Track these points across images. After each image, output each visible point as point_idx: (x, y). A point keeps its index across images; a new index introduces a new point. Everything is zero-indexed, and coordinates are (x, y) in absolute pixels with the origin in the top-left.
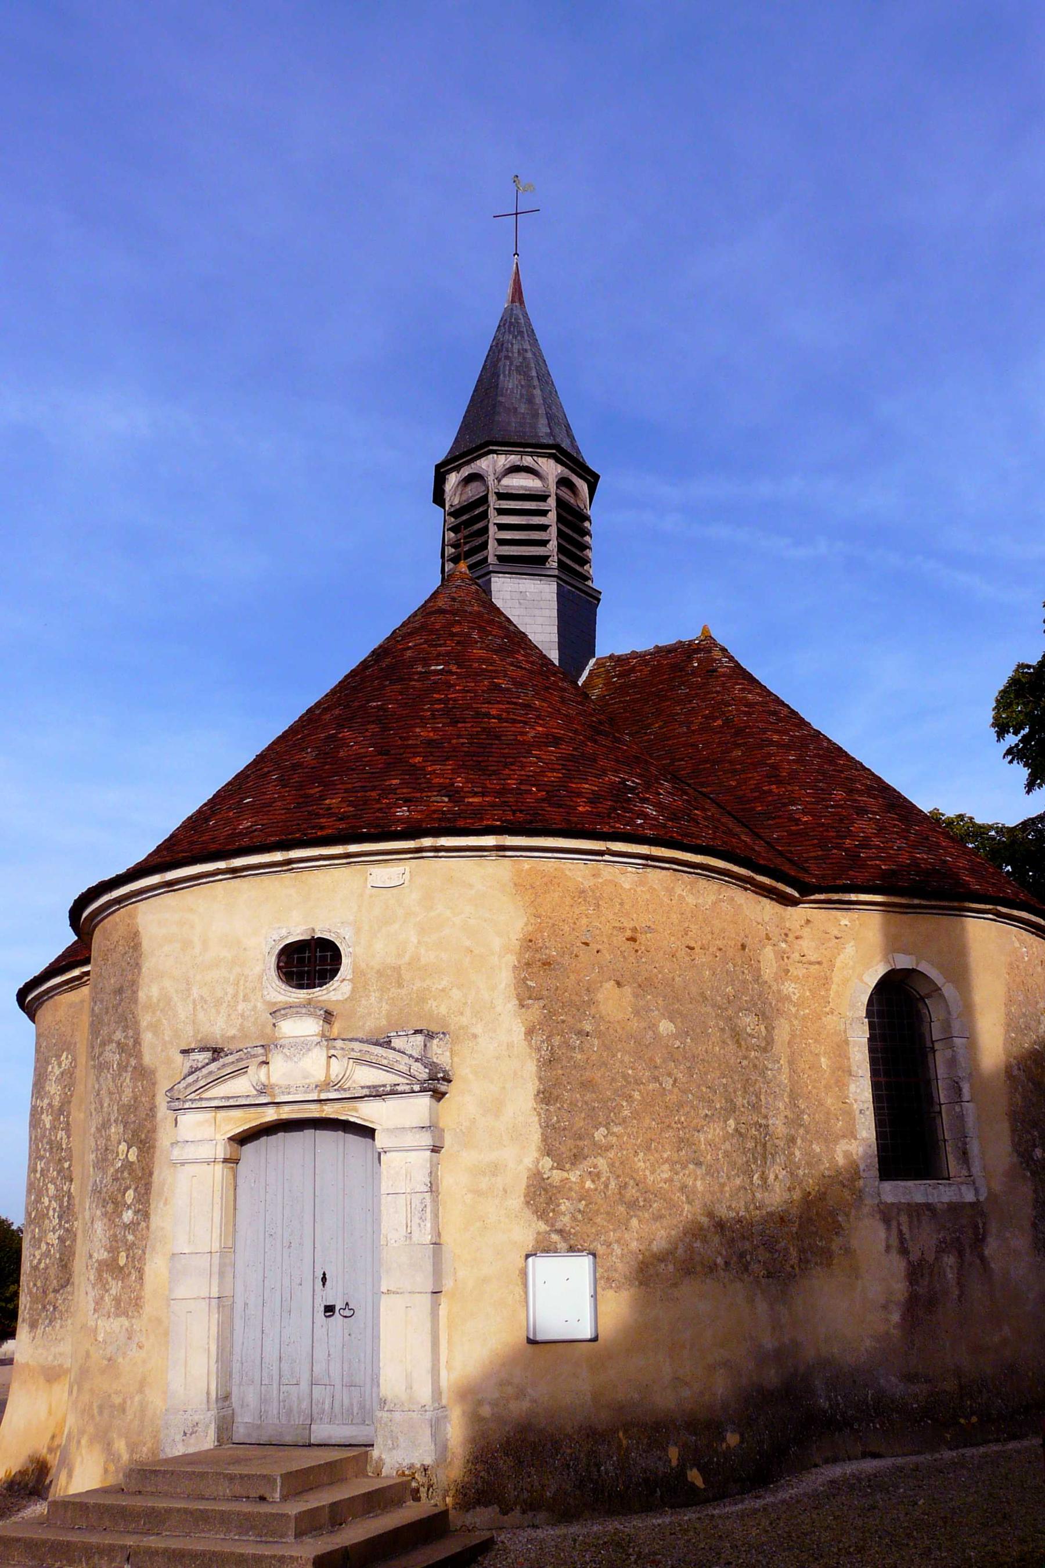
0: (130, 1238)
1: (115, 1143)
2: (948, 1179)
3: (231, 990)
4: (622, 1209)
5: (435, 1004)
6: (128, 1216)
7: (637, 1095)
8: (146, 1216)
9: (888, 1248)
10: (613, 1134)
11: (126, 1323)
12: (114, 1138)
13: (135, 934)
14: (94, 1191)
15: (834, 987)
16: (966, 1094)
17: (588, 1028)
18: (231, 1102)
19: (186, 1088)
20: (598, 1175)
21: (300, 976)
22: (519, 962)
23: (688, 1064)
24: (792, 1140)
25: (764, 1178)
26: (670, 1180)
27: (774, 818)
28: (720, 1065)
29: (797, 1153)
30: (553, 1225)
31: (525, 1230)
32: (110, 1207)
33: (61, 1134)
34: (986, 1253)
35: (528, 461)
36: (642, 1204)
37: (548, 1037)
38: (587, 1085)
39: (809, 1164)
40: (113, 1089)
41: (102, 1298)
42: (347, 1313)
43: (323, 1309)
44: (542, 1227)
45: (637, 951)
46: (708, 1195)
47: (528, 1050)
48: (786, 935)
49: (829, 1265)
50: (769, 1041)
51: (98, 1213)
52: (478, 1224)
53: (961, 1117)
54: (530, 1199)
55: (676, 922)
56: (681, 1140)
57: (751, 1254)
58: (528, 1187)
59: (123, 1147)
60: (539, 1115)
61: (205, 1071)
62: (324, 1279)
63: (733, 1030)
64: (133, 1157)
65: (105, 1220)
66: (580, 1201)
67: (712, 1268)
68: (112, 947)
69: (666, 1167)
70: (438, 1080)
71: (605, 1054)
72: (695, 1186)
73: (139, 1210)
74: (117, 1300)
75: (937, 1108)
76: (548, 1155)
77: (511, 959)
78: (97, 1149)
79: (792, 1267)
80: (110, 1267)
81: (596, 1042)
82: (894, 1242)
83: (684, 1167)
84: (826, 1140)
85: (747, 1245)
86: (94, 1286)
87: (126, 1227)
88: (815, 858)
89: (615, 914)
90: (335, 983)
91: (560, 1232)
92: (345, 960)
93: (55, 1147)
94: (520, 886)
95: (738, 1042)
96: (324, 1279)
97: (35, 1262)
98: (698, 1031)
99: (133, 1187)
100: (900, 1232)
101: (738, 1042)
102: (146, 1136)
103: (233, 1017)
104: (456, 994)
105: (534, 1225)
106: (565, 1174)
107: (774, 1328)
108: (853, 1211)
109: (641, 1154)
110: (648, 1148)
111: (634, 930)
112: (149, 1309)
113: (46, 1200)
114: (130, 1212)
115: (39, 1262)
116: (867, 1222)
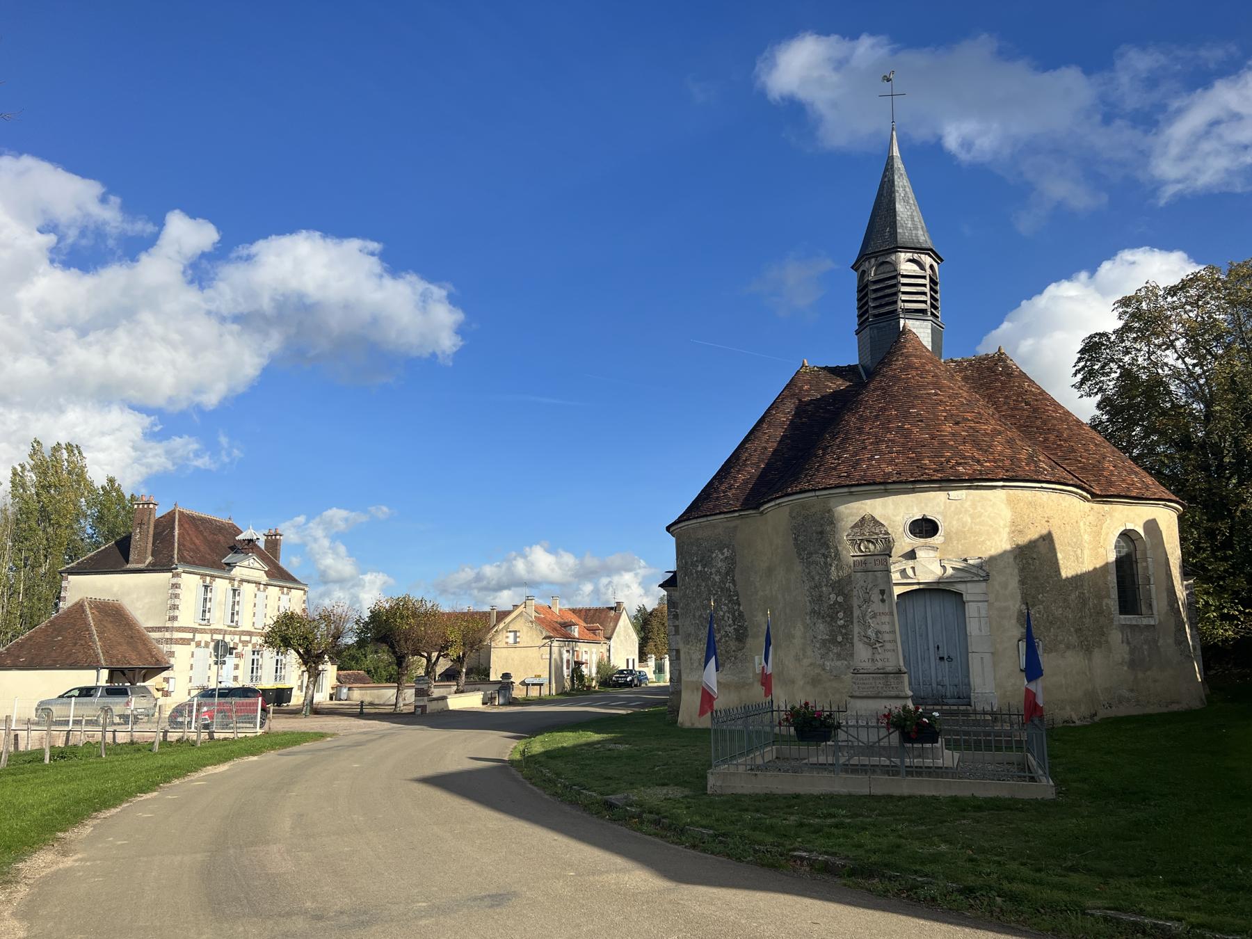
21: (921, 532)
32: (828, 619)
38: (1036, 578)
53: (1149, 590)
77: (1007, 530)
94: (1009, 501)
104: (988, 543)
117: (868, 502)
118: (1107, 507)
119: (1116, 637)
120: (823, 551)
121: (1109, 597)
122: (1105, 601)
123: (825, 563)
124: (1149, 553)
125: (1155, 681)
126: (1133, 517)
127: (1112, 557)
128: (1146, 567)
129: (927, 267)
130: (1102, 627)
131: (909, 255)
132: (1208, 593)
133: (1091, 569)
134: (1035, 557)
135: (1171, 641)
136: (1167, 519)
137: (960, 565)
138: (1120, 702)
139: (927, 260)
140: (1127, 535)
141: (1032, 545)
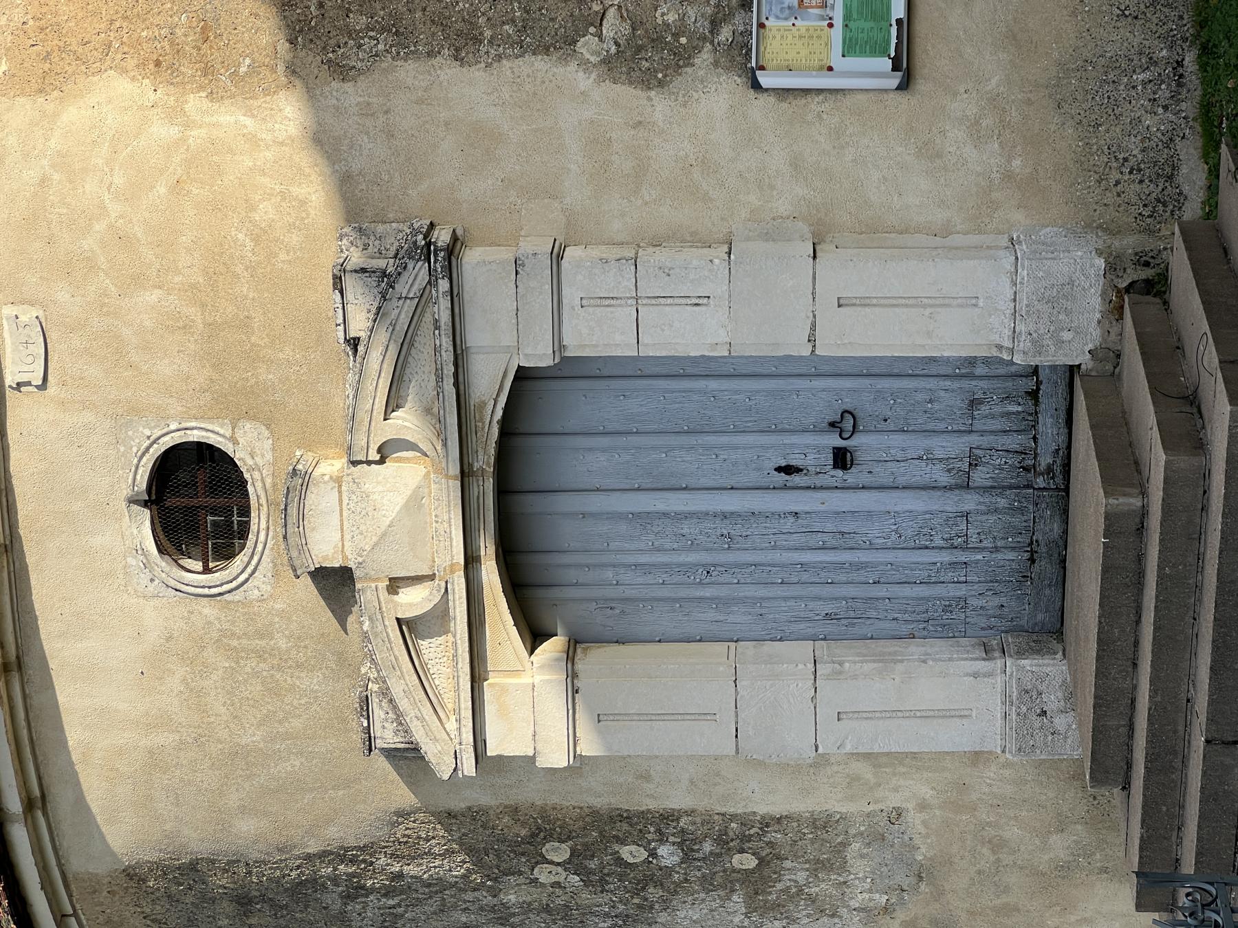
0: (707, 847)
3: (250, 665)
6: (668, 855)
8: (669, 817)
11: (856, 846)
13: (130, 877)
18: (457, 319)
22: (201, 88)
31: (712, 96)
32: (653, 893)
37: (350, 37)
40: (433, 905)
41: (812, 900)
43: (839, 473)
44: (705, 57)
52: (696, 174)
54: (649, 81)
58: (631, 83)
59: (543, 875)
60: (499, 57)
61: (403, 704)
62: (788, 470)
64: (559, 852)
70: (428, 244)
73: (659, 831)
76: (575, 42)
77: (195, 103)
87: (687, 858)
90: (240, 456)
91: (715, 25)
92: (195, 436)
99: (616, 847)
102: (524, 824)
103: (301, 657)
104: (266, 211)
105: (701, 73)
106: (612, 12)
112: (826, 798)
114: (663, 851)
117: (75, 736)
120: (332, 899)
123: (388, 892)
137: (379, 363)
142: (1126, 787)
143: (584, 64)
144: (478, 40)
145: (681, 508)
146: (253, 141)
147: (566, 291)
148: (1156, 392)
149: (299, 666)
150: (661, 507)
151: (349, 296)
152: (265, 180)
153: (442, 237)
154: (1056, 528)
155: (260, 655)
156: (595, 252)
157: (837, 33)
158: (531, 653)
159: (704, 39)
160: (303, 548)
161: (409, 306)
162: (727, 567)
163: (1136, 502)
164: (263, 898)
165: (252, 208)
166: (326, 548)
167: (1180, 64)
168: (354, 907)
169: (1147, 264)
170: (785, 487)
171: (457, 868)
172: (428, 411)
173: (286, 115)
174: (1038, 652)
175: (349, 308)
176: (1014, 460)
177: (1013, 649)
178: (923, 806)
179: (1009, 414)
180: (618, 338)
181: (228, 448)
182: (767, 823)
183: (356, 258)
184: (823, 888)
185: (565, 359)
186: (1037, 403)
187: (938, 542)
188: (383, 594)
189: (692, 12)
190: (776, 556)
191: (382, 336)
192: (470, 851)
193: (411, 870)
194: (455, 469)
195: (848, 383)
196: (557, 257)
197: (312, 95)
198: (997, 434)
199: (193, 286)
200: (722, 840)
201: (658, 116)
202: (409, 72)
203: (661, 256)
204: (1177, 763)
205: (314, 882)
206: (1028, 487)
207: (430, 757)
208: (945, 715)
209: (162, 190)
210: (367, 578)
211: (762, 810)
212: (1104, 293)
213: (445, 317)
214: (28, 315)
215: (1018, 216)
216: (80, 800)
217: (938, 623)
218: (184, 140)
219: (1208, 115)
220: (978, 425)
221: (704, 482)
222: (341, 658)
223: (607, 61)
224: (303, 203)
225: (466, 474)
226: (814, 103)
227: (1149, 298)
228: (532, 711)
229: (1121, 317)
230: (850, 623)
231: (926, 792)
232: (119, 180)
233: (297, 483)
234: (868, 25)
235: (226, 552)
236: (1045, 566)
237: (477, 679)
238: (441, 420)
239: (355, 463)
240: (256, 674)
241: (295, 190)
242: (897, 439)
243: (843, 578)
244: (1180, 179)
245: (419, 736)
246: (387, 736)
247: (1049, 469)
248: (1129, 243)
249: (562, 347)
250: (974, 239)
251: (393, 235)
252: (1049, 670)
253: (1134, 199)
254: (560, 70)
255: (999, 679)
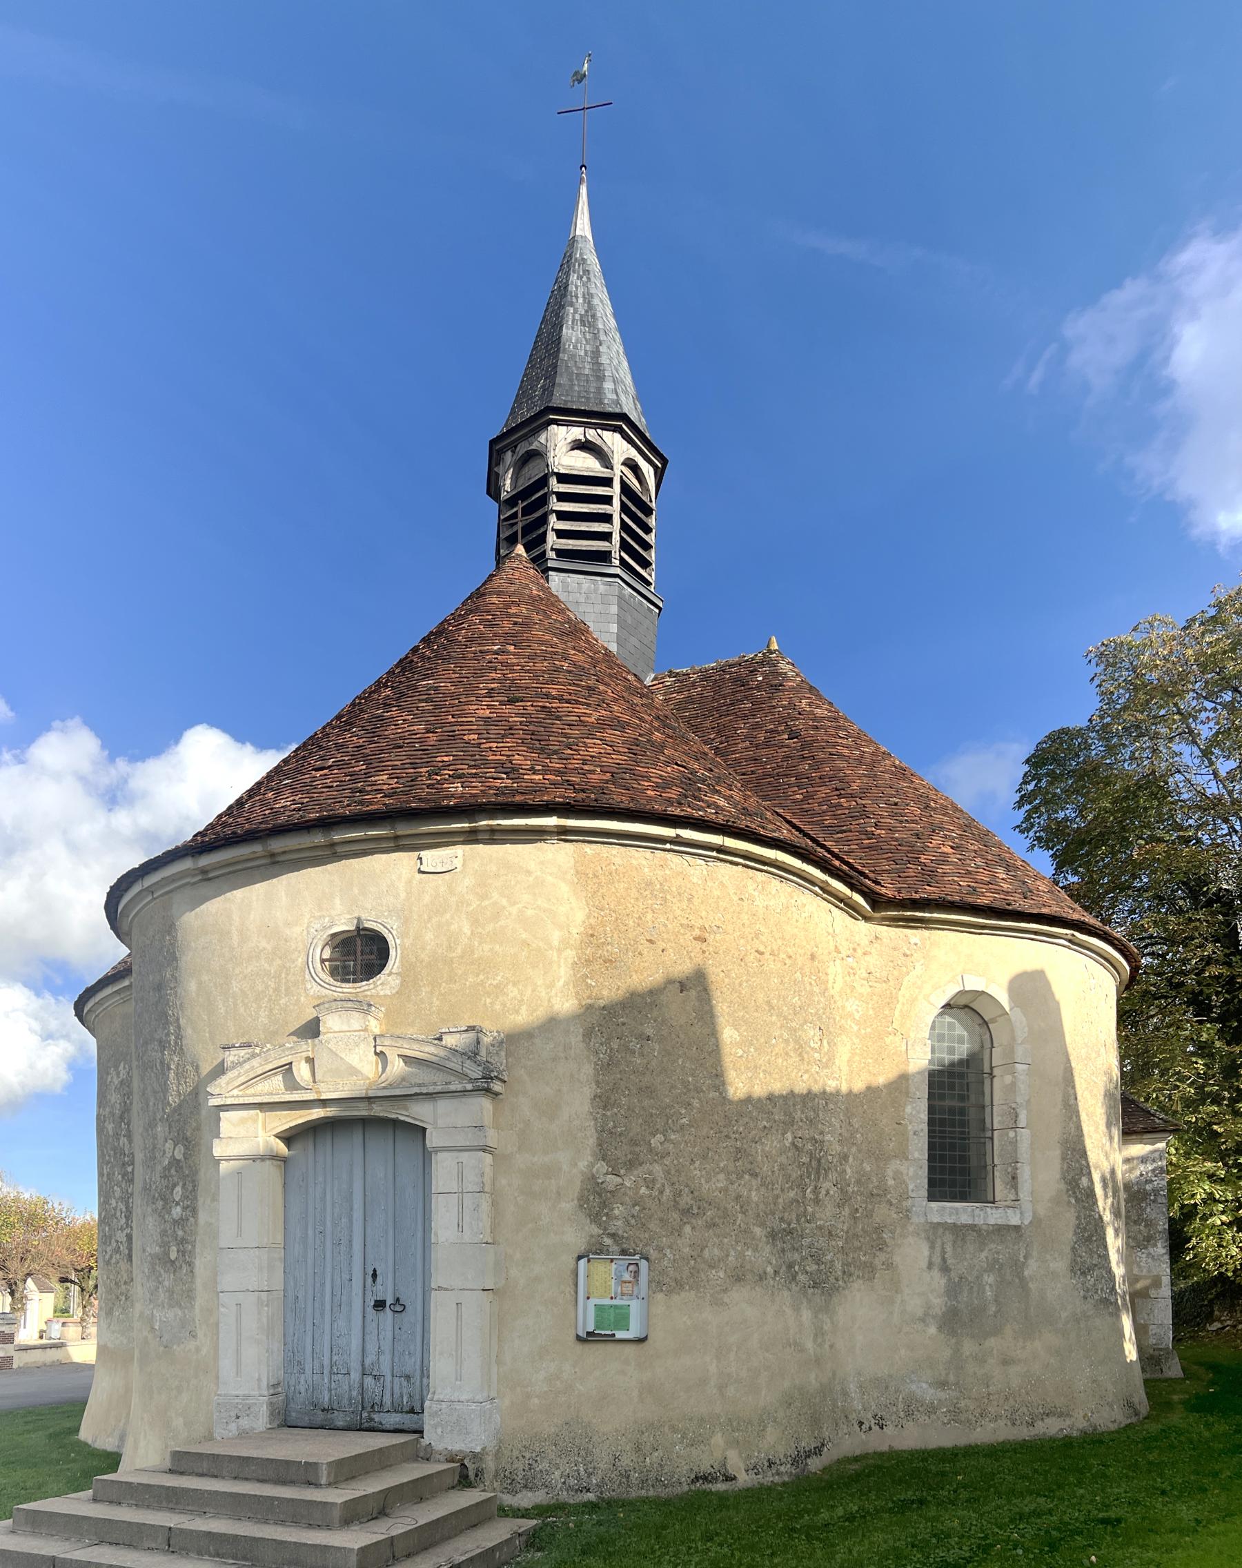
0: (180, 1233)
1: (161, 1141)
2: (993, 1203)
4: (676, 1215)
5: (488, 1001)
6: (177, 1211)
7: (696, 1103)
8: (194, 1212)
9: (930, 1266)
10: (671, 1141)
12: (161, 1136)
14: (145, 1189)
15: (899, 1007)
16: (1022, 1121)
17: (649, 1031)
19: (228, 1083)
20: (654, 1180)
22: (579, 958)
23: (750, 1074)
24: (845, 1157)
25: (816, 1190)
26: (726, 1190)
27: (845, 831)
28: (781, 1077)
29: (849, 1171)
30: (605, 1229)
31: (576, 1236)
32: (160, 1204)
33: (124, 1140)
34: (1026, 1273)
35: (591, 434)
36: (695, 1211)
38: (649, 1091)
39: (858, 1182)
42: (398, 1308)
43: (372, 1303)
44: (596, 1230)
45: (704, 952)
46: (762, 1206)
47: (586, 1052)
48: (855, 950)
49: (871, 1279)
50: (831, 1059)
51: (149, 1209)
53: (1014, 1143)
54: (583, 1200)
55: (747, 923)
56: (738, 1150)
57: (800, 1265)
60: (595, 1119)
61: (247, 1066)
62: (374, 1275)
63: (796, 1041)
65: (156, 1216)
66: (634, 1206)
67: (762, 1277)
68: (148, 942)
69: (722, 1176)
71: (665, 1060)
72: (749, 1197)
74: (171, 1292)
75: (989, 1134)
77: (571, 954)
78: (145, 1148)
79: (837, 1279)
80: (163, 1260)
81: (657, 1047)
82: (937, 1260)
83: (740, 1177)
84: (877, 1159)
85: (796, 1256)
86: (148, 1278)
87: (176, 1222)
88: (888, 872)
89: (683, 910)
90: (381, 978)
91: (613, 1236)
92: (392, 952)
93: (119, 1152)
94: (582, 876)
95: (800, 1055)
96: (374, 1275)
97: (107, 1257)
98: (762, 1040)
100: (944, 1252)
101: (800, 1055)
104: (513, 992)
106: (619, 1180)
107: (816, 1335)
108: (898, 1230)
109: (697, 1164)
110: (705, 1157)
111: (703, 928)
112: (201, 1299)
113: (113, 1202)
114: (179, 1209)
115: (111, 1257)
116: (911, 1239)
117: (239, 894)
118: (915, 936)
119: (912, 1254)
120: (160, 1034)
121: (903, 1155)
122: (895, 1165)
124: (1019, 1054)
125: (1006, 1362)
126: (989, 961)
127: (920, 1059)
128: (1011, 1091)
129: (617, 460)
130: (879, 1230)
131: (577, 433)
132: (1211, 1177)
133: (859, 1086)
134: (647, 1040)
135: (1060, 1265)
136: (1081, 990)
137: (427, 1051)
138: (909, 1414)
139: (618, 447)
140: (965, 1007)
141: (639, 1005)
142: (171, 1471)
143: (592, 1165)
144: (605, 1108)
145: (355, 1216)
146: (551, 986)
147: (466, 1154)
148: (387, 1492)
149: (271, 1010)
150: (356, 1206)
151: (464, 1035)
152: (529, 992)
153: (497, 1086)
154: (340, 1424)
155: (277, 990)
156: (488, 1171)
157: (607, 1302)
158: (277, 1136)
159: (605, 1229)
160: (330, 1011)
161: (458, 1068)
162: (323, 1243)
163: (324, 1481)
164: (160, 997)
165: (514, 984)
166: (332, 1023)
167: (588, 1490)
168: (156, 1045)
169: (477, 1475)
170: (365, 1274)
171: (173, 1099)
172: (403, 1079)
173: (565, 1004)
174: (272, 1414)
175: (458, 1035)
176: (377, 1400)
177: (274, 1399)
178: (198, 1350)
179: (402, 1397)
180: (441, 1183)
181: (386, 971)
182: (190, 1264)
183: (486, 1040)
184: (162, 1296)
185: (430, 1153)
186: (407, 1412)
187: (335, 1358)
188: (305, 1055)
189: (619, 1223)
190: (328, 1269)
191: (442, 1053)
192: (180, 1105)
193: (172, 1075)
194: (371, 1094)
195: (419, 1308)
196: (485, 1149)
197: (575, 1018)
198: (392, 1390)
199: (473, 952)
200: (183, 1241)
201: (563, 1205)
202: (588, 1070)
203: (485, 1206)
204: (171, 1505)
205: (167, 1023)
206: (363, 1408)
207: (218, 1081)
208: (238, 1364)
209: (524, 936)
210: (314, 1046)
211: (197, 1262)
212: (461, 1451)
213: (452, 1087)
214: (459, 866)
215: (507, 1402)
216: (207, 899)
217: (292, 1360)
218: (551, 948)
219: (558, 1508)
220: (396, 1380)
221: (369, 1230)
222: (275, 1033)
223: (593, 1177)
224: (517, 1012)
225: (369, 1099)
226: (569, 1289)
227: (457, 1478)
228: (243, 1137)
229: (448, 1461)
230: (294, 1310)
231: (204, 1351)
232: (530, 912)
233: (364, 1007)
234: (612, 1318)
235: (334, 972)
236: (320, 1417)
237: (261, 1106)
238: (391, 1086)
239: (375, 1039)
240: (267, 987)
241: (524, 1008)
242: (389, 1335)
243: (317, 1305)
244: (524, 1492)
245: (230, 1075)
246: (231, 1057)
247: (372, 1420)
248: (490, 1465)
249: (436, 1152)
250: (495, 1377)
251: (499, 1061)
252: (261, 1421)
253: (515, 1466)
254: (588, 1152)
255: (256, 1393)
